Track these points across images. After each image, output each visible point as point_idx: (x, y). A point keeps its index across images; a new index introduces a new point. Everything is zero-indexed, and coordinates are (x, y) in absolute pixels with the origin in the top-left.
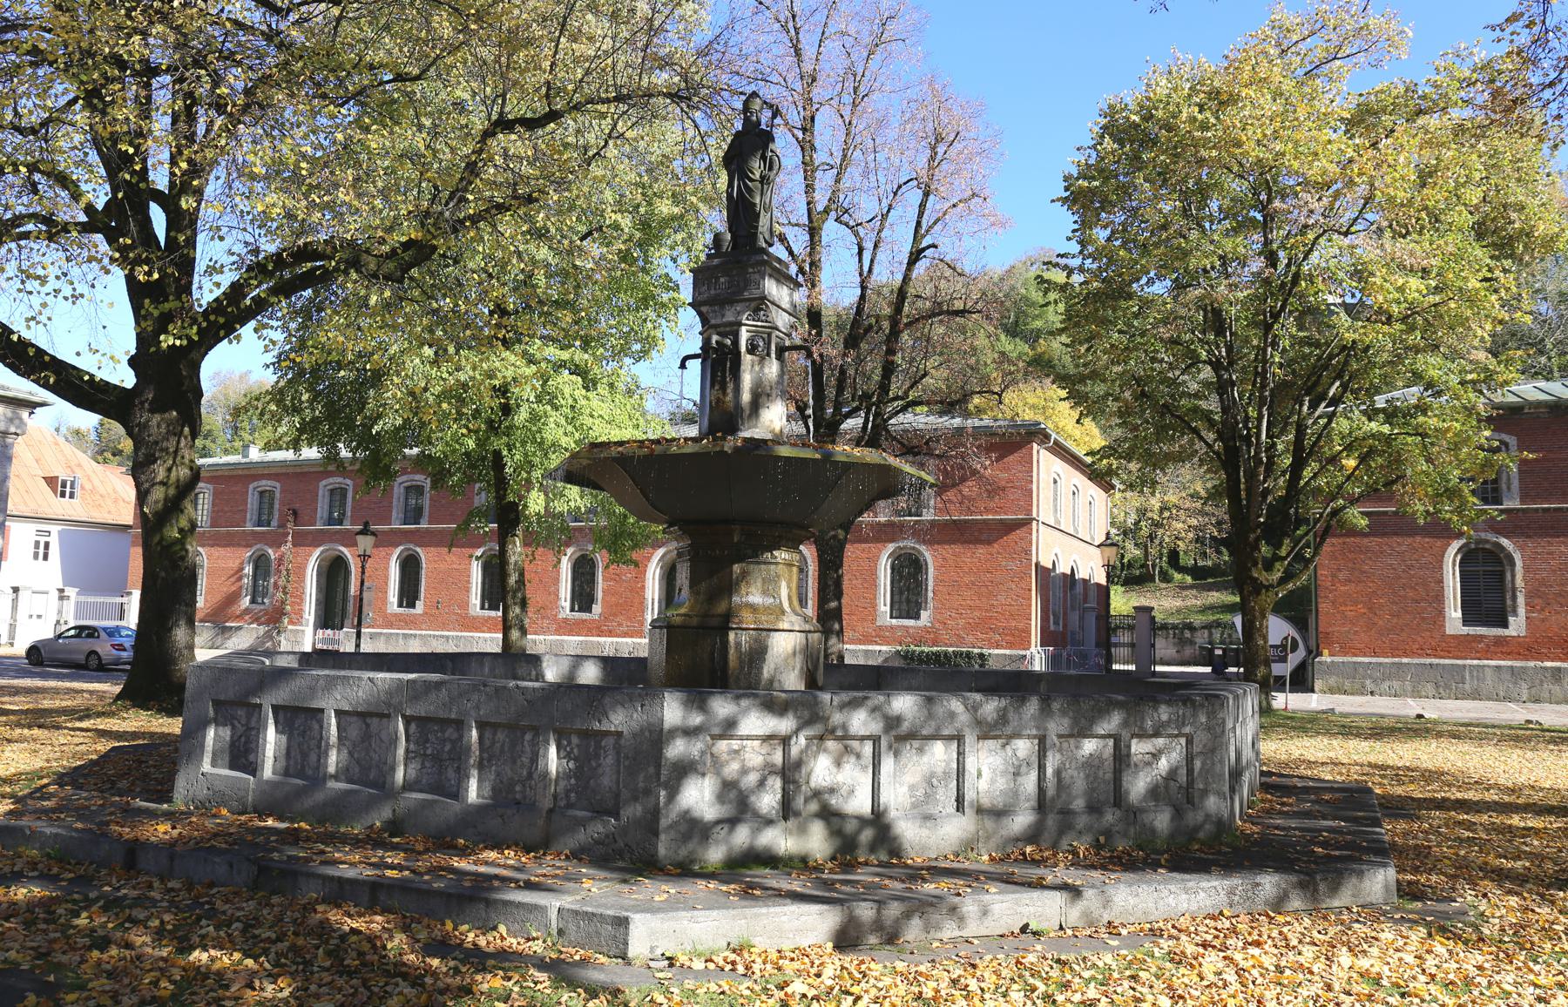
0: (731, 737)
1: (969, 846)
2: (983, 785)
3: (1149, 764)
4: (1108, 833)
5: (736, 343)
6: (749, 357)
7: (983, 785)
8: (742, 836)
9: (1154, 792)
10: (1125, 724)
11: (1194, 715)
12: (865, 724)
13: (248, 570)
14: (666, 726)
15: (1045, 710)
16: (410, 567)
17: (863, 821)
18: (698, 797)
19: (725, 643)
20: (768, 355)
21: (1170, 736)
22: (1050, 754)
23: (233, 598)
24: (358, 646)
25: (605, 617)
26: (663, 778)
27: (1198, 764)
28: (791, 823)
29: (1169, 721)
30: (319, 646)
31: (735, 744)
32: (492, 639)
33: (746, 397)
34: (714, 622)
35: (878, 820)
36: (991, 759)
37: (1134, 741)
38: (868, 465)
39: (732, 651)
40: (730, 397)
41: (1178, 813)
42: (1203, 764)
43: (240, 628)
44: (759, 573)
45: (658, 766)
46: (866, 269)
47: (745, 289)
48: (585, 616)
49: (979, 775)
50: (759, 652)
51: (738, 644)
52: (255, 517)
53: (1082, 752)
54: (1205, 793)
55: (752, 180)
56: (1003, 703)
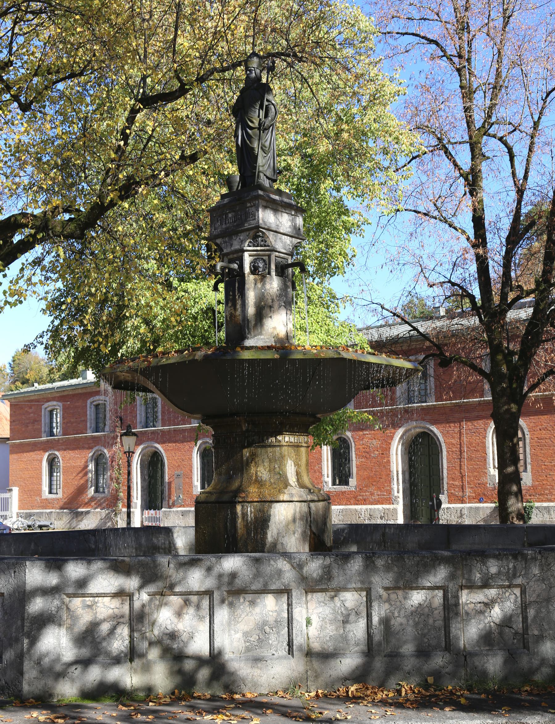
0: (84, 595)
1: (294, 685)
2: (313, 631)
3: (481, 612)
4: (437, 674)
5: (241, 266)
6: (252, 277)
7: (313, 631)
8: (94, 674)
9: (488, 639)
10: (452, 577)
11: (527, 568)
12: (202, 582)
13: (91, 466)
14: (28, 588)
15: (370, 565)
16: (52, 462)
17: (201, 661)
18: (56, 643)
19: (234, 513)
20: (269, 273)
21: (502, 587)
22: (375, 605)
23: (81, 490)
24: (129, 523)
25: (360, 488)
26: (26, 629)
27: (531, 612)
28: (137, 663)
29: (499, 573)
30: (146, 523)
31: (89, 601)
32: (183, 514)
33: (251, 310)
34: (226, 498)
35: (215, 662)
36: (321, 610)
37: (465, 592)
38: (325, 359)
39: (240, 521)
40: (239, 312)
41: (511, 657)
42: (538, 612)
43: (88, 513)
44: (265, 454)
45: (23, 619)
46: (520, 174)
47: (246, 221)
48: (343, 488)
49: (309, 622)
50: (262, 522)
51: (244, 515)
52: (93, 425)
53: (410, 602)
54: (540, 638)
55: (251, 128)
56: (328, 561)
